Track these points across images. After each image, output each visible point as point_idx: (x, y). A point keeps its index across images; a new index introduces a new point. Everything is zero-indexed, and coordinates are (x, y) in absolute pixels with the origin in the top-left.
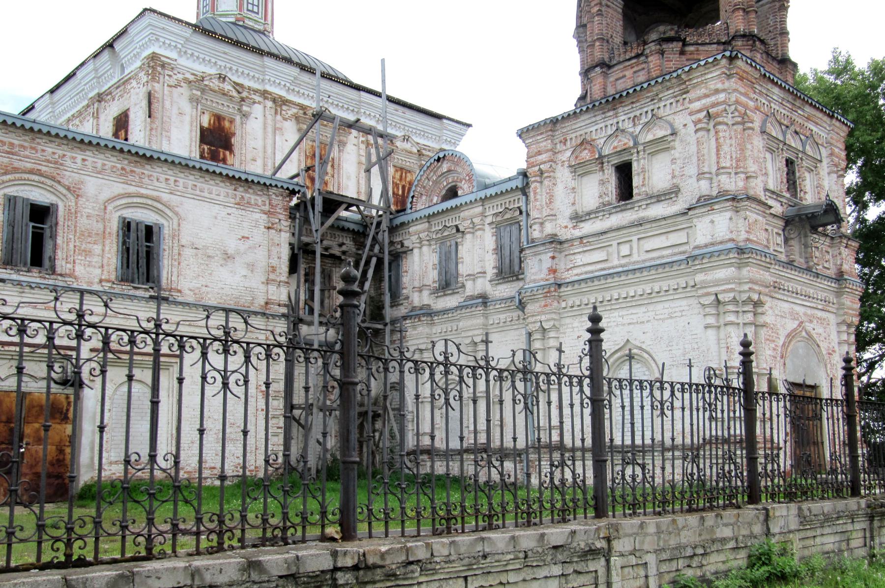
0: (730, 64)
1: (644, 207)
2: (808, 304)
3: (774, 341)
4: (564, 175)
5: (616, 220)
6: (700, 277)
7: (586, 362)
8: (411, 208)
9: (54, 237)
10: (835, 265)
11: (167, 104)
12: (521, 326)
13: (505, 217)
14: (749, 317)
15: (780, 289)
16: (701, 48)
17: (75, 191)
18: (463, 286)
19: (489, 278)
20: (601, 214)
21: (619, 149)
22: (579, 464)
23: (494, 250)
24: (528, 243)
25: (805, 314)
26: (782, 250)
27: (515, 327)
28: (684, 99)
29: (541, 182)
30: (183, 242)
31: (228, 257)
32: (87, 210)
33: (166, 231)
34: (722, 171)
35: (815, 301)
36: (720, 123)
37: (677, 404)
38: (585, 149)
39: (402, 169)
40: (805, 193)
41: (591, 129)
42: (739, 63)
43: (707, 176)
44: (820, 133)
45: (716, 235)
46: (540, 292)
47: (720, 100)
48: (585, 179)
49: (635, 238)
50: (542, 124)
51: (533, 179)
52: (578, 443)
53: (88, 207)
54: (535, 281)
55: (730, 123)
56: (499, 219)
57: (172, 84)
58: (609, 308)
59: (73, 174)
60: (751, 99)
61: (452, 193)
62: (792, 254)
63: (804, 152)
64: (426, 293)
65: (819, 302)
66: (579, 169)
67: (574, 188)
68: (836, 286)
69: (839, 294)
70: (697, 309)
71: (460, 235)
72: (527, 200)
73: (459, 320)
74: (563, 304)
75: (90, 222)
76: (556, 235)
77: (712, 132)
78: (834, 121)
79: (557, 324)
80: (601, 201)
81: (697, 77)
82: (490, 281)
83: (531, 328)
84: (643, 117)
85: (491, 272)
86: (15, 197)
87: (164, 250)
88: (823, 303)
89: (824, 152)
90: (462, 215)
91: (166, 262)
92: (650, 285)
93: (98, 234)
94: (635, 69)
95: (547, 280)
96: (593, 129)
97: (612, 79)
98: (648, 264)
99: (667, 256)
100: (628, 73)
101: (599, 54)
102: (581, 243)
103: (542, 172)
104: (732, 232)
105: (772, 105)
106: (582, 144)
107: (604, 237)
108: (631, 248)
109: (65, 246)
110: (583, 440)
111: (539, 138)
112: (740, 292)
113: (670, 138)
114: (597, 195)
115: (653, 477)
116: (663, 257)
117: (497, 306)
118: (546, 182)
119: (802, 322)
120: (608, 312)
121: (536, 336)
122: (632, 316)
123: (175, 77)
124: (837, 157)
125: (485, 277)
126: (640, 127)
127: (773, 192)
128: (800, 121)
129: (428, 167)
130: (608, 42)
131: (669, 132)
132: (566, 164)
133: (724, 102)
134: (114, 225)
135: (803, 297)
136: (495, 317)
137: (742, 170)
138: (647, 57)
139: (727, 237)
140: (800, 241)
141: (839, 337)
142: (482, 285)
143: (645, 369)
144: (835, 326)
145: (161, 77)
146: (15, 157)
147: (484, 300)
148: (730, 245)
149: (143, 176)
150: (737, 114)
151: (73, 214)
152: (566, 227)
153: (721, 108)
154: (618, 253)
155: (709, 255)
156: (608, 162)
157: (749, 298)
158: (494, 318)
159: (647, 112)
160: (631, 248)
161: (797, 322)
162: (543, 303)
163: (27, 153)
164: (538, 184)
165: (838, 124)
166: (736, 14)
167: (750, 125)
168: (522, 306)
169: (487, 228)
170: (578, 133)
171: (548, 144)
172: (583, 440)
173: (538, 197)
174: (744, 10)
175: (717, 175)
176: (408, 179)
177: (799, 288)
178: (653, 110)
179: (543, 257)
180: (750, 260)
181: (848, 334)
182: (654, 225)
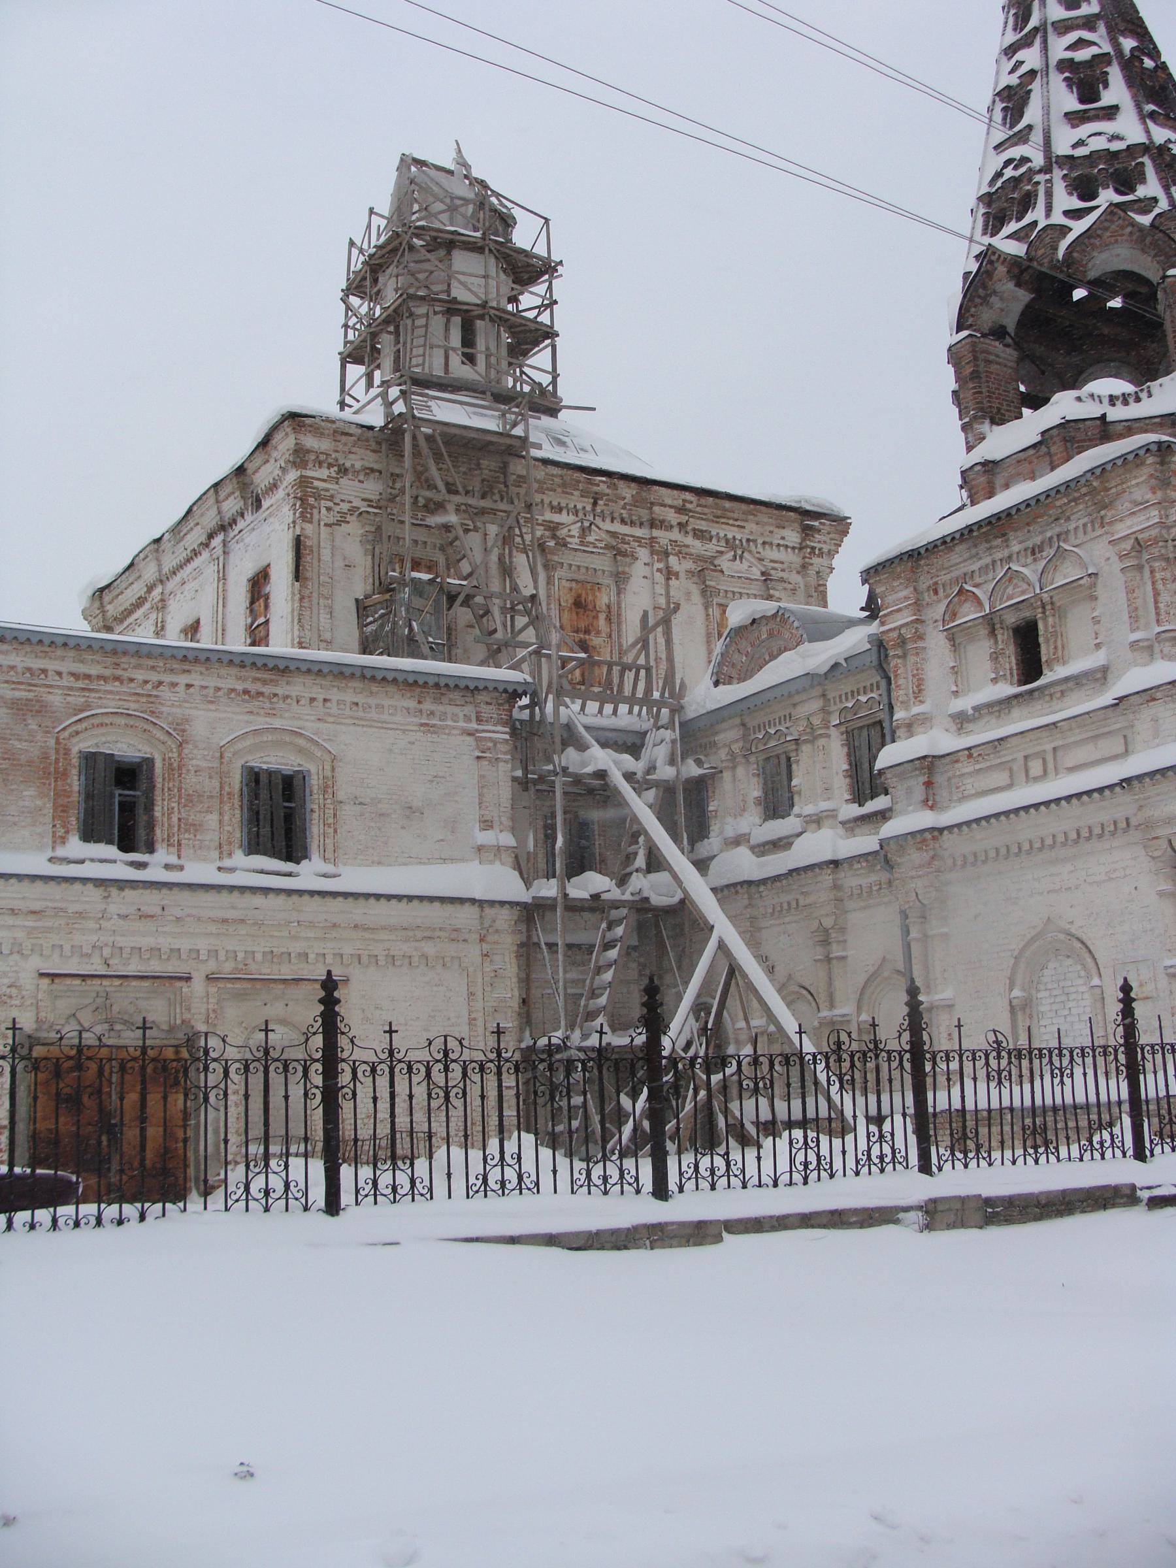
4: (936, 643)
9: (150, 807)
11: (326, 554)
17: (180, 735)
22: (296, 1164)
30: (341, 795)
31: (411, 811)
32: (194, 762)
33: (314, 782)
37: (474, 1091)
53: (198, 758)
57: (331, 520)
59: (174, 710)
75: (201, 779)
86: (94, 754)
87: (312, 811)
91: (315, 830)
93: (211, 797)
102: (970, 756)
109: (165, 819)
118: (911, 659)
123: (337, 508)
134: (236, 781)
145: (315, 511)
146: (93, 695)
149: (275, 700)
151: (176, 770)
154: (1027, 771)
163: (109, 687)
164: (899, 661)
169: (834, 732)
179: (912, 782)
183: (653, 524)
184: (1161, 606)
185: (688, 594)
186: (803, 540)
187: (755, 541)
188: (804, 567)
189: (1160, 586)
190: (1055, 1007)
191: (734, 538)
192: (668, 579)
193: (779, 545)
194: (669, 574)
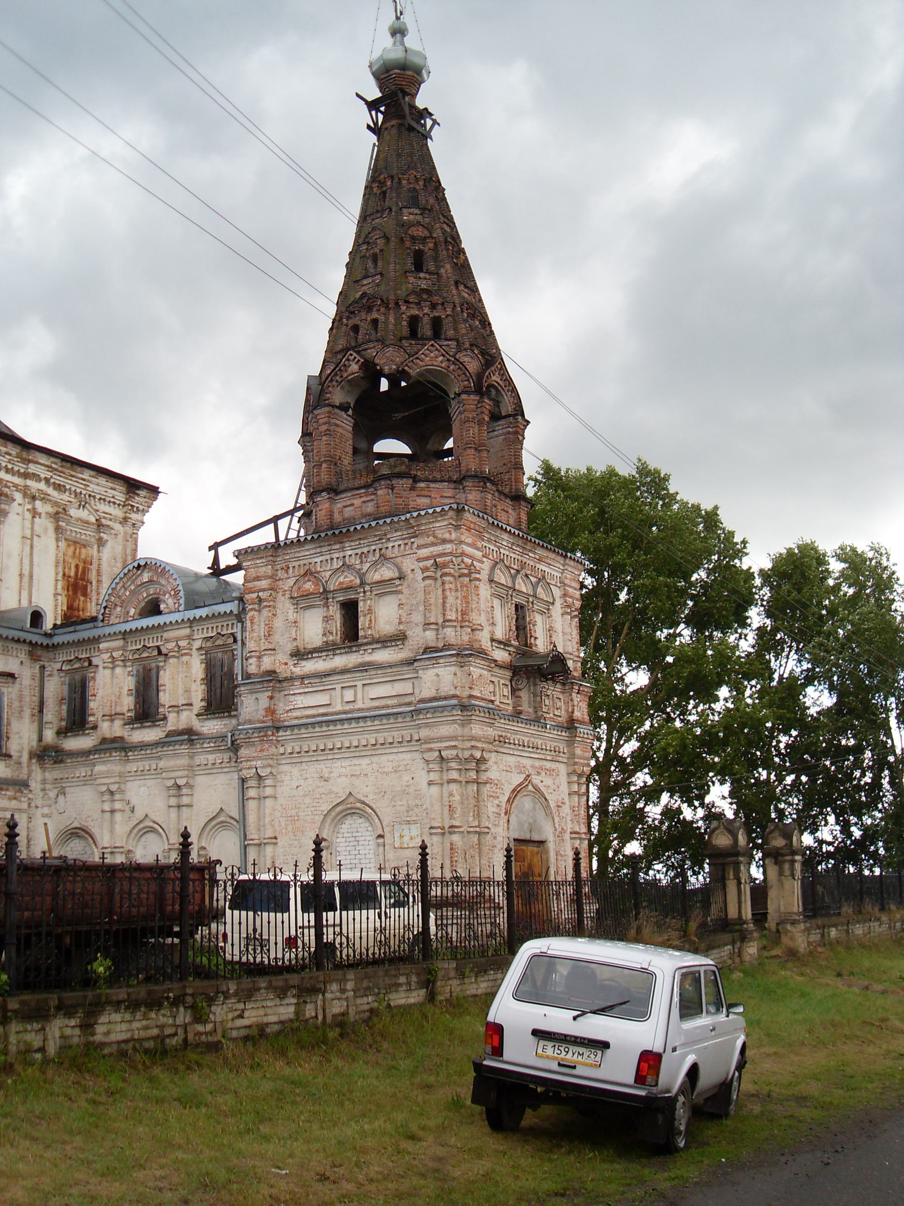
0: (457, 516)
1: (370, 651)
2: (536, 756)
3: (498, 797)
5: (339, 661)
6: (424, 733)
7: (311, 872)
8: (103, 621)
10: (567, 711)
12: (232, 769)
13: (217, 643)
14: (473, 774)
15: (505, 742)
16: (432, 485)
18: (165, 718)
19: (196, 711)
20: (324, 654)
21: (344, 586)
23: (202, 679)
24: (242, 679)
25: (532, 766)
26: (509, 702)
27: (226, 770)
28: (412, 543)
29: (259, 611)
34: (447, 624)
35: (544, 752)
36: (446, 574)
38: (309, 580)
39: (75, 543)
40: (536, 638)
41: (316, 560)
42: (467, 515)
43: (433, 627)
44: (553, 573)
45: (441, 689)
46: (256, 735)
47: (446, 551)
48: (309, 613)
49: (359, 684)
50: (263, 548)
51: (251, 607)
52: (306, 924)
54: (250, 722)
55: (457, 575)
56: (209, 644)
58: (331, 757)
60: (478, 549)
61: (153, 608)
62: (519, 706)
63: (535, 596)
64: (118, 723)
65: (548, 753)
66: (302, 601)
67: (295, 622)
68: (567, 734)
69: (571, 743)
70: (421, 764)
71: (162, 658)
72: (242, 627)
73: (160, 758)
74: (282, 750)
76: (274, 672)
77: (439, 582)
78: (568, 561)
79: (274, 771)
80: (325, 639)
81: (426, 524)
82: (197, 715)
83: (245, 773)
84: (370, 555)
85: (199, 704)
88: (553, 753)
89: (557, 592)
90: (165, 635)
92: (375, 735)
94: (363, 499)
95: (263, 722)
96: (318, 560)
97: (339, 505)
98: (372, 713)
99: (393, 707)
100: (357, 502)
101: (325, 477)
103: (260, 600)
104: (456, 688)
105: (502, 551)
106: (305, 575)
107: (327, 679)
108: (355, 695)
110: (309, 921)
111: (258, 562)
112: (463, 749)
113: (397, 582)
114: (320, 632)
115: (354, 945)
116: (388, 707)
117: (205, 745)
119: (528, 776)
120: (331, 761)
121: (252, 783)
122: (355, 768)
124: (571, 597)
125: (191, 710)
126: (368, 565)
127: (500, 642)
128: (531, 563)
129: (125, 574)
130: (336, 464)
131: (397, 575)
132: (288, 596)
133: (451, 554)
135: (531, 749)
136: (202, 757)
137: (467, 623)
138: (376, 490)
139: (451, 693)
140: (529, 690)
141: (569, 788)
142: (186, 719)
143: (367, 824)
144: (565, 776)
147: (189, 736)
148: (454, 702)
150: (463, 566)
152: (286, 664)
153: (448, 558)
154: (342, 697)
155: (432, 710)
156: (333, 598)
157: (472, 755)
158: (200, 759)
159: (374, 550)
160: (355, 695)
161: (524, 776)
162: (259, 748)
164: (256, 613)
165: (572, 563)
166: (468, 451)
167: (478, 576)
168: (235, 748)
169: (194, 652)
170: (302, 562)
171: (269, 570)
172: (309, 921)
173: (255, 627)
174: (476, 449)
175: (443, 627)
176: (83, 556)
177: (526, 739)
178: (381, 549)
180: (473, 717)
181: (579, 784)
182: (379, 672)
183: (26, 476)
184: (448, 605)
185: (46, 530)
186: (127, 499)
187: (94, 497)
188: (126, 519)
189: (448, 593)
190: (348, 849)
191: (81, 493)
192: (34, 517)
193: (110, 502)
194: (35, 513)
